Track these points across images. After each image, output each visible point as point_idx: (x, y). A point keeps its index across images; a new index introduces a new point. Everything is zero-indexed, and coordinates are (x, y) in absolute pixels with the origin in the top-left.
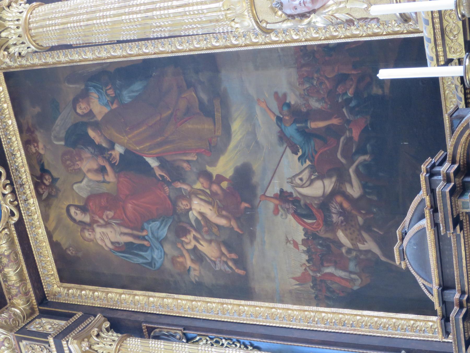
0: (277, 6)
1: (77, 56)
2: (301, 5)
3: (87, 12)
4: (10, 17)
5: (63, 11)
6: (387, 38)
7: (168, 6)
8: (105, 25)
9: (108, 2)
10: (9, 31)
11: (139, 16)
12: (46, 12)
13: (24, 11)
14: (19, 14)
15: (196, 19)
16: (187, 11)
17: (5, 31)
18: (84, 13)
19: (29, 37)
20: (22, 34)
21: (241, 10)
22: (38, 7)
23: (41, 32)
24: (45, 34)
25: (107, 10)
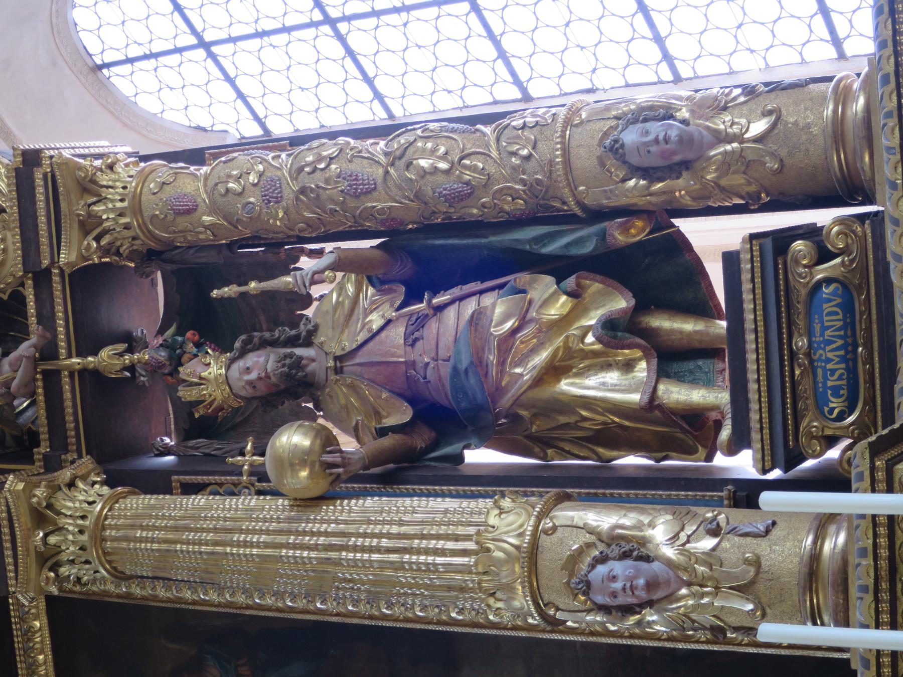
0: (580, 586)
1: (189, 592)
2: (625, 592)
3: (216, 529)
4: (69, 508)
5: (170, 518)
6: (789, 654)
7: (372, 546)
8: (247, 560)
9: (258, 516)
10: (65, 535)
11: (313, 554)
12: (139, 511)
13: (98, 501)
14: (87, 505)
15: (422, 579)
16: (406, 562)
17: (56, 533)
18: (211, 529)
19: (100, 552)
20: (88, 545)
21: (510, 578)
22: (124, 498)
23: (124, 549)
24: (132, 554)
25: (254, 532)
